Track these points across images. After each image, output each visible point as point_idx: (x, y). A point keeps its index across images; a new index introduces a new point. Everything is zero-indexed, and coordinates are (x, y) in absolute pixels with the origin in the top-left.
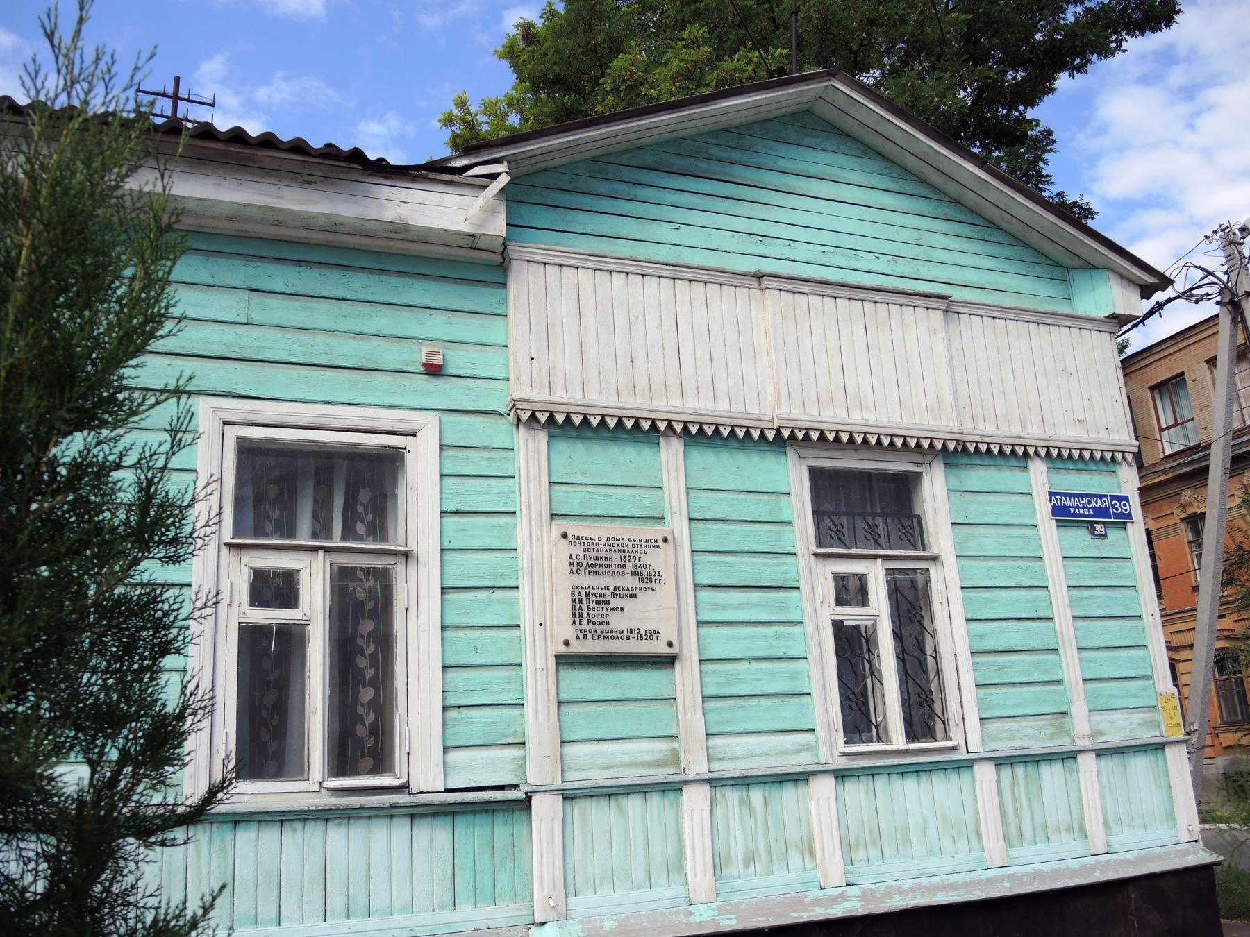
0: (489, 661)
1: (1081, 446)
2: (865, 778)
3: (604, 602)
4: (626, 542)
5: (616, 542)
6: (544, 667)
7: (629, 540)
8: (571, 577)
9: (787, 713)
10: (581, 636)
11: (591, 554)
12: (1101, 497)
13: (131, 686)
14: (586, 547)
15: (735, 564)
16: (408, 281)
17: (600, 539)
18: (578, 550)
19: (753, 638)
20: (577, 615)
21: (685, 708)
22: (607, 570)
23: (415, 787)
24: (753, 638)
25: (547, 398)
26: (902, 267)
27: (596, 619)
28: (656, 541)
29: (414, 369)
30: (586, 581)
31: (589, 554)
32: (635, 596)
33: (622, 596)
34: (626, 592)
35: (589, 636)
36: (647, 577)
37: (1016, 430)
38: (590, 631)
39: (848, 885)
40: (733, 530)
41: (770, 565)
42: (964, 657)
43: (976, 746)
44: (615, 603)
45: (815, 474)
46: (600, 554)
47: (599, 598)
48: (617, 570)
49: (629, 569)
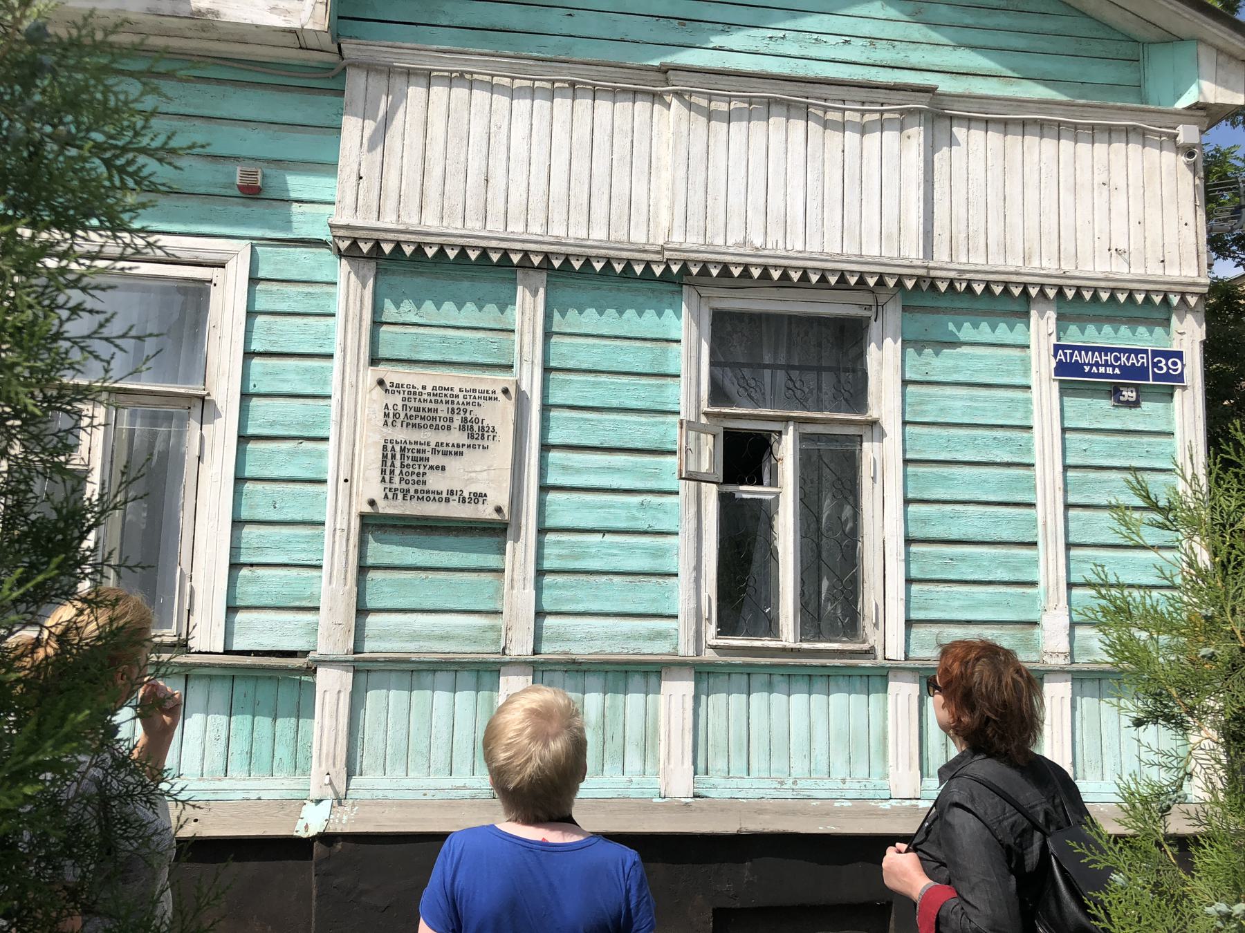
0: (289, 517)
1: (1112, 285)
2: (738, 676)
3: (421, 459)
4: (456, 392)
5: (444, 392)
6: (345, 527)
7: (461, 390)
8: (385, 430)
9: (643, 596)
10: (390, 495)
11: (412, 404)
12: (1137, 352)
13: (34, 522)
14: (406, 395)
15: (599, 421)
16: (230, 89)
17: (424, 387)
18: (397, 399)
19: (610, 507)
20: (388, 472)
21: (512, 580)
22: (429, 423)
23: (194, 644)
24: (610, 507)
25: (372, 223)
26: (882, 54)
27: (410, 478)
28: (494, 392)
29: (229, 192)
30: (401, 434)
31: (409, 404)
32: (462, 454)
33: (445, 453)
34: (450, 449)
35: (400, 496)
36: (479, 434)
37: (1015, 263)
38: (402, 490)
39: (695, 796)
40: (600, 383)
41: (645, 424)
42: (896, 546)
43: (895, 651)
44: (435, 460)
45: (959, 331)
46: (422, 405)
47: (416, 455)
48: (442, 423)
49: (457, 423)
